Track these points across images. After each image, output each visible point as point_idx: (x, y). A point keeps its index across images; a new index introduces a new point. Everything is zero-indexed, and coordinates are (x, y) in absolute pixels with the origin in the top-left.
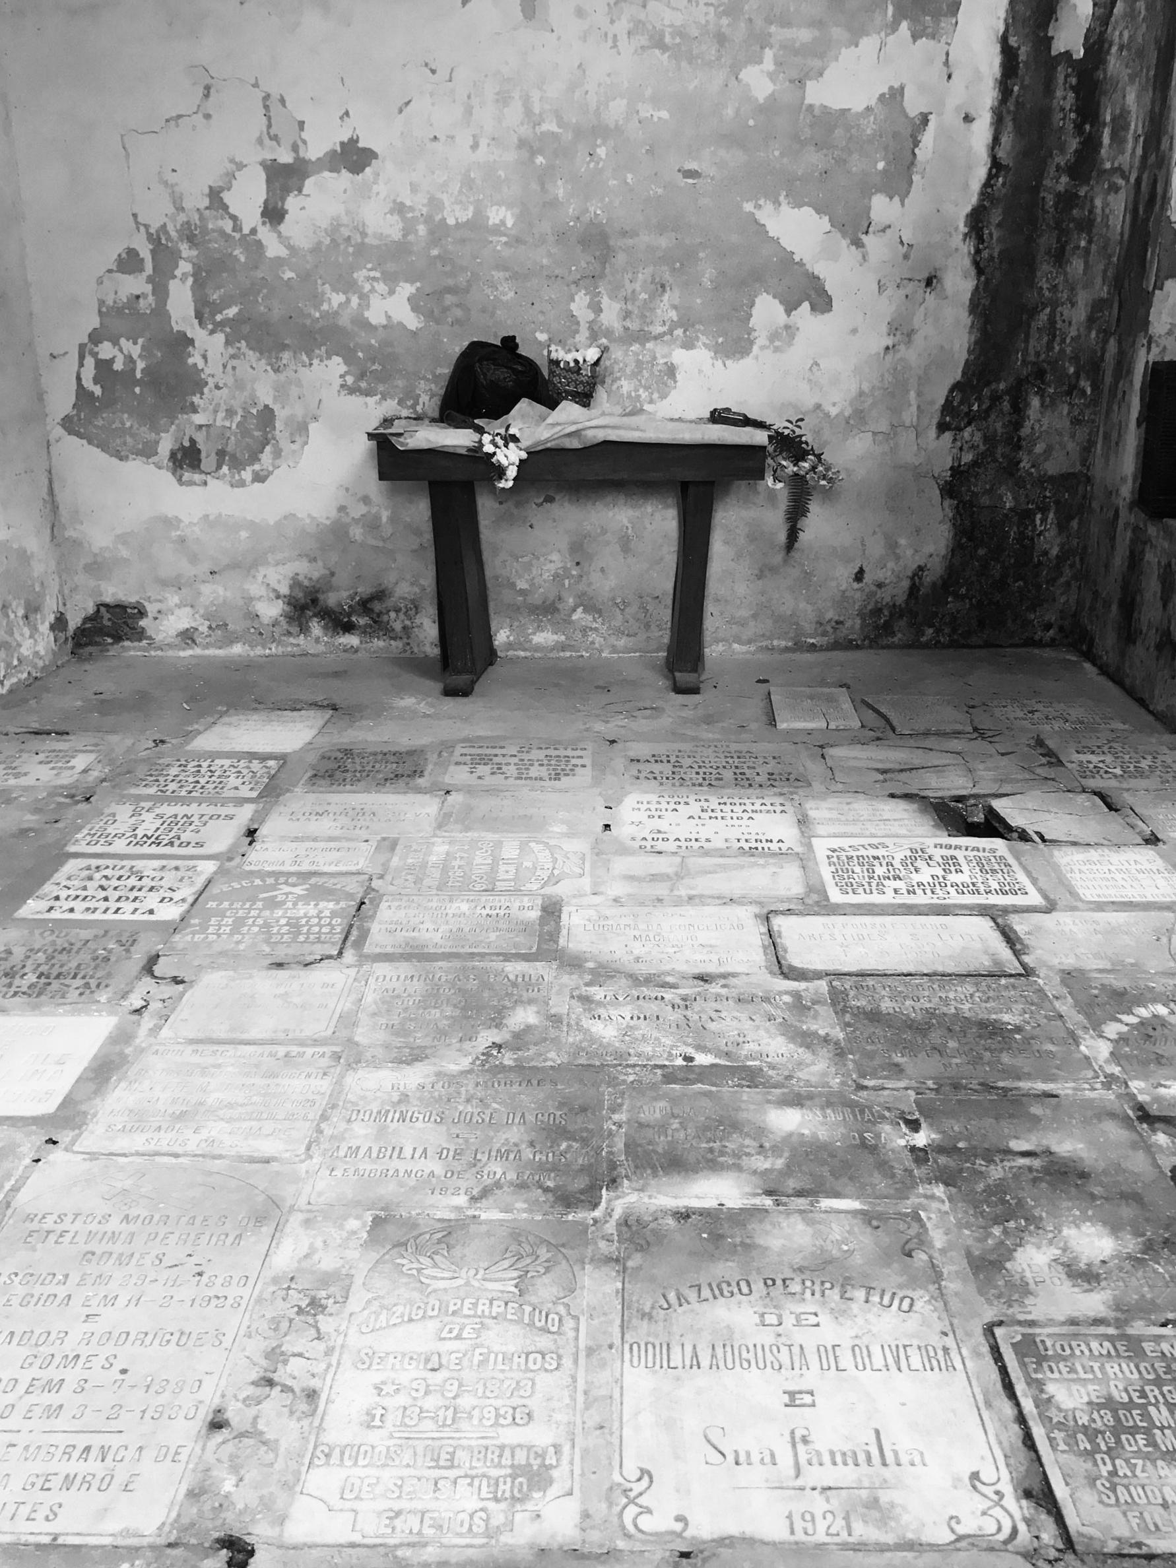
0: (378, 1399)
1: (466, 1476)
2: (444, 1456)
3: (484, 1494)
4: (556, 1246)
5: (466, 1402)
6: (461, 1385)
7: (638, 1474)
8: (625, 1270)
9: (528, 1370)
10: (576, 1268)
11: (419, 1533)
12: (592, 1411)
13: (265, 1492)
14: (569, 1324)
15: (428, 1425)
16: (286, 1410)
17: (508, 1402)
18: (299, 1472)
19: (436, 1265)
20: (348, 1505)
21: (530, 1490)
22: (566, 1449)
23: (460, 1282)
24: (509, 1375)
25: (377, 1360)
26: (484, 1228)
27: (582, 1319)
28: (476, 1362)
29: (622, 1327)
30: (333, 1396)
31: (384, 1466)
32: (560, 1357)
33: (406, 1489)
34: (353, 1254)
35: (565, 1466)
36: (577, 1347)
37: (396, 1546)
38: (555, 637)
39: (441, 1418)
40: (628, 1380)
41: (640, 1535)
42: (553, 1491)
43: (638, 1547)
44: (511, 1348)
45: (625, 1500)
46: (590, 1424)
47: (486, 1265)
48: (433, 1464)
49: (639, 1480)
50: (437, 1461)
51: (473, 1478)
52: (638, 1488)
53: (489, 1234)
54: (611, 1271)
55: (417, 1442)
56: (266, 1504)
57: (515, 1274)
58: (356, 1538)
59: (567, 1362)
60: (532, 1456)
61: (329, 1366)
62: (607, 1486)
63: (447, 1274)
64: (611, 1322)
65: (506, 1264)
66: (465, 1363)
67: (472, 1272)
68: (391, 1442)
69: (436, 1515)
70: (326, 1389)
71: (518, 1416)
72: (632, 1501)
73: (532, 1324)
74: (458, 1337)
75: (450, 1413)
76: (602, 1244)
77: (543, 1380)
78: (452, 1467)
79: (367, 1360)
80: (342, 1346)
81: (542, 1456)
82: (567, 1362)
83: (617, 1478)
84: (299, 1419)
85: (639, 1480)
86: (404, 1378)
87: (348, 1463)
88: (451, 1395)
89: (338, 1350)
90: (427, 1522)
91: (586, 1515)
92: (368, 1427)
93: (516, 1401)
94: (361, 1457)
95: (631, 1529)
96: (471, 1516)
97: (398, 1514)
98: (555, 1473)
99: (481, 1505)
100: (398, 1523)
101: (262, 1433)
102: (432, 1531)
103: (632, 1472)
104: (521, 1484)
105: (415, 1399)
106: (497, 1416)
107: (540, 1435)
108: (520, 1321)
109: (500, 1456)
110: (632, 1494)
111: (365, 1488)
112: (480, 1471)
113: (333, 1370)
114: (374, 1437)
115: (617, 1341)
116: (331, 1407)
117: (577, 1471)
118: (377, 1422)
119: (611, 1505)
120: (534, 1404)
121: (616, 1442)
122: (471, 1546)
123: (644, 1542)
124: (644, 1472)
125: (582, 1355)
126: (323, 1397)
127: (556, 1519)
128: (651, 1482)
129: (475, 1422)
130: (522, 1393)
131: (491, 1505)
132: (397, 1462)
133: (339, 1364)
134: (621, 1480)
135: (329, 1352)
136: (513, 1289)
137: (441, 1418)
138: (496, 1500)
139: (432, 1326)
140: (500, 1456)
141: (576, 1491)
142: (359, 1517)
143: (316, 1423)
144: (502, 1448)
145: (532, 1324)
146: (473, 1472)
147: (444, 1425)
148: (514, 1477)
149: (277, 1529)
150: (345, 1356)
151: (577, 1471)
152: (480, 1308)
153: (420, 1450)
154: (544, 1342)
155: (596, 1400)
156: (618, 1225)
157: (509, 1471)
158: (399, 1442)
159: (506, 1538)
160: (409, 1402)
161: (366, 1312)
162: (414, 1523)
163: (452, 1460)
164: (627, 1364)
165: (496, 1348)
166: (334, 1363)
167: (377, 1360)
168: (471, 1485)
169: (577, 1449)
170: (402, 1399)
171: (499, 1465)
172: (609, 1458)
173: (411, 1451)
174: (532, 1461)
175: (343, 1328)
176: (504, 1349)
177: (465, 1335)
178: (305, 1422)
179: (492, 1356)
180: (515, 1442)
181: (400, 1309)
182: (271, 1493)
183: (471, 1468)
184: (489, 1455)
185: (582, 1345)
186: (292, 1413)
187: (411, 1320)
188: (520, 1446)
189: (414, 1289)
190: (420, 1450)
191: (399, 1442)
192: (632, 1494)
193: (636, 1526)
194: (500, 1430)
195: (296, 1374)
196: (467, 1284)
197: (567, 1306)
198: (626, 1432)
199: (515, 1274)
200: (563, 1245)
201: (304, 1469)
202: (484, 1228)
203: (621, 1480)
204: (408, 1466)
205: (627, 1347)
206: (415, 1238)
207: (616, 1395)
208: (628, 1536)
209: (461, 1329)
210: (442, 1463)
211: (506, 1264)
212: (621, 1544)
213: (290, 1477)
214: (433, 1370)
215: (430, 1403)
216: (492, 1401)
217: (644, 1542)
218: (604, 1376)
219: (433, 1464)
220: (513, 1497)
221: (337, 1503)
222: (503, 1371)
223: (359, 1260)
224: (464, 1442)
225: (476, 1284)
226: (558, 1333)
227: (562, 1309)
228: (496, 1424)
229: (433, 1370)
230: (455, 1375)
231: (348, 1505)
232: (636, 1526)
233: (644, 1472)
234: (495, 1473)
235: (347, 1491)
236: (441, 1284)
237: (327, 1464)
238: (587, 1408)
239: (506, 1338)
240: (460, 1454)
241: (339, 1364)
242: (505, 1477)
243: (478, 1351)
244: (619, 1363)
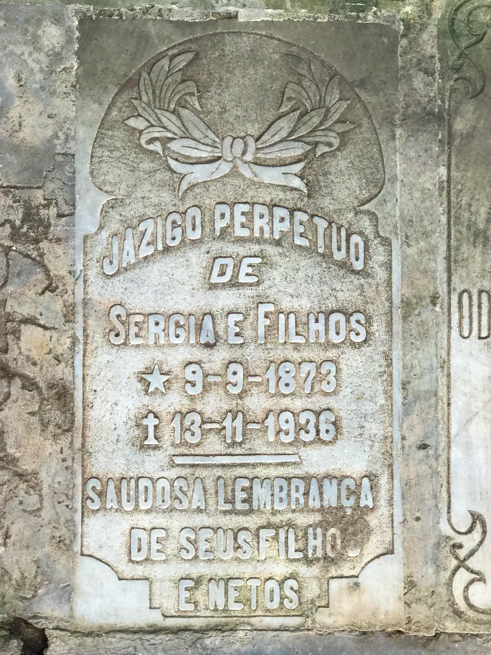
0: (146, 400)
1: (268, 526)
2: (241, 496)
3: (293, 555)
4: (351, 85)
5: (256, 403)
6: (247, 375)
7: (469, 520)
8: (451, 135)
9: (329, 345)
10: (383, 136)
11: (225, 610)
12: (414, 418)
13: (39, 554)
14: (379, 256)
15: (214, 445)
16: (34, 419)
17: (308, 403)
18: (70, 522)
19: (187, 135)
20: (140, 571)
21: (344, 548)
22: (383, 481)
23: (225, 168)
24: (306, 354)
25: (134, 330)
26: (246, 42)
27: (396, 244)
28: (261, 331)
29: (448, 258)
30: (90, 396)
31: (171, 510)
32: (369, 320)
33: (203, 546)
34: (65, 106)
35: (383, 509)
36: (390, 299)
37: (204, 631)
38: (152, 165)
39: (228, 433)
40: (457, 361)
41: (471, 613)
42: (374, 546)
43: (470, 629)
44: (304, 304)
45: (454, 563)
46: (412, 440)
47: (254, 129)
48: (228, 507)
49: (470, 531)
50: (232, 501)
51: (277, 527)
52: (469, 542)
53: (254, 58)
54: (430, 141)
55: (204, 473)
56: (43, 570)
57: (298, 150)
58: (155, 618)
59: (378, 327)
60: (344, 493)
61: (74, 340)
62: (433, 541)
63: (205, 153)
64: (432, 251)
65: (284, 126)
66: (248, 333)
67: (239, 145)
68: (173, 473)
69: (240, 583)
70: (79, 381)
71: (323, 428)
72: (462, 563)
73: (327, 256)
74: (234, 284)
75: (239, 422)
76: (419, 81)
77: (352, 362)
78: (251, 511)
79: (123, 328)
80: (85, 303)
81: (355, 493)
82: (378, 327)
83: (445, 529)
84: (55, 437)
85: (470, 531)
86: (174, 359)
87: (128, 507)
88: (236, 391)
89: (79, 309)
90: (233, 594)
91: (410, 584)
92: (142, 447)
93: (319, 402)
94: (142, 498)
95: (462, 605)
96: (281, 583)
97: (198, 582)
98: (373, 520)
99: (291, 568)
100: (199, 596)
101: (14, 461)
102: (239, 607)
103: (462, 522)
104: (334, 537)
105: (192, 398)
106: (299, 428)
107: (350, 459)
108: (310, 251)
109: (306, 494)
110: (462, 553)
111: (155, 546)
112: (285, 518)
113: (80, 347)
114: (153, 464)
115: (442, 290)
116: (92, 414)
117: (398, 518)
118: (151, 441)
119: (439, 568)
120: (342, 405)
121: (442, 470)
122: (286, 629)
123: (478, 623)
124: (477, 519)
125: (397, 314)
126: (78, 395)
127: (375, 589)
128: (484, 532)
129: (271, 438)
130: (325, 387)
131: (303, 570)
132: (185, 505)
133: (86, 336)
134: (450, 533)
135: (69, 316)
136: (297, 183)
137: (228, 433)
138: (309, 562)
139: (196, 258)
140: (306, 494)
141: (398, 548)
142: (156, 587)
143: (78, 444)
144: (307, 479)
145: (327, 256)
146: (277, 519)
147: (234, 444)
148: (325, 525)
149: (66, 608)
150: (90, 322)
151: (398, 518)
152: (258, 223)
153: (209, 484)
154: (346, 291)
155: (417, 398)
156: (441, 34)
157: (317, 517)
158: (184, 472)
159: (323, 618)
160: (184, 404)
161: (105, 234)
162: (216, 595)
163: (248, 501)
164: (455, 333)
165: (286, 304)
166: (80, 334)
167: (134, 330)
168: (276, 538)
169: (396, 482)
170: (175, 401)
171: (306, 509)
172: (435, 497)
173: (198, 486)
174: (346, 503)
175: (79, 267)
176: (296, 304)
177: (243, 279)
178: (64, 442)
179: (282, 317)
180: (322, 471)
181: (149, 226)
182: (48, 556)
183: (274, 513)
184: (294, 494)
185: (397, 300)
186: (45, 425)
187: (167, 249)
188: (329, 477)
189: (162, 185)
190: (209, 484)
191: (184, 472)
192: (462, 553)
193: (466, 598)
194: (304, 452)
195: (35, 354)
196: (234, 173)
197: (373, 216)
198: (456, 454)
199: (298, 150)
200: (362, 84)
201: (78, 517)
202: (246, 42)
203: (450, 533)
204: (199, 510)
205: (455, 298)
206: (151, 66)
207: (442, 392)
208: (458, 614)
209: (237, 267)
210: (239, 506)
211: (284, 126)
212: (451, 626)
213: (63, 531)
214: (208, 346)
215: (213, 404)
216: (286, 402)
217: (478, 623)
218: (425, 356)
219: (228, 507)
220: (326, 557)
221: (128, 570)
222: (297, 347)
223: (80, 120)
224: (261, 472)
225: (246, 171)
226: (364, 273)
227: (366, 223)
228: (296, 442)
229: (208, 346)
230: (237, 354)
231: (140, 571)
232: (466, 598)
233: (477, 519)
234: (302, 520)
235: (134, 551)
236: (199, 174)
237: (103, 508)
238: (407, 413)
239: (295, 285)
240: (260, 493)
241: (86, 336)
242: (314, 526)
243: (263, 309)
244: (444, 328)
